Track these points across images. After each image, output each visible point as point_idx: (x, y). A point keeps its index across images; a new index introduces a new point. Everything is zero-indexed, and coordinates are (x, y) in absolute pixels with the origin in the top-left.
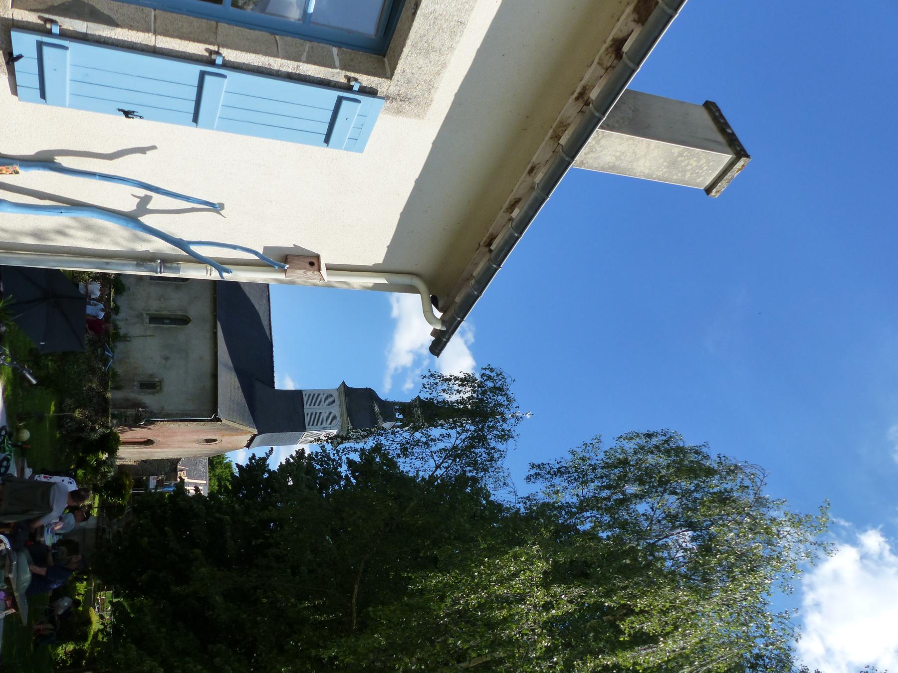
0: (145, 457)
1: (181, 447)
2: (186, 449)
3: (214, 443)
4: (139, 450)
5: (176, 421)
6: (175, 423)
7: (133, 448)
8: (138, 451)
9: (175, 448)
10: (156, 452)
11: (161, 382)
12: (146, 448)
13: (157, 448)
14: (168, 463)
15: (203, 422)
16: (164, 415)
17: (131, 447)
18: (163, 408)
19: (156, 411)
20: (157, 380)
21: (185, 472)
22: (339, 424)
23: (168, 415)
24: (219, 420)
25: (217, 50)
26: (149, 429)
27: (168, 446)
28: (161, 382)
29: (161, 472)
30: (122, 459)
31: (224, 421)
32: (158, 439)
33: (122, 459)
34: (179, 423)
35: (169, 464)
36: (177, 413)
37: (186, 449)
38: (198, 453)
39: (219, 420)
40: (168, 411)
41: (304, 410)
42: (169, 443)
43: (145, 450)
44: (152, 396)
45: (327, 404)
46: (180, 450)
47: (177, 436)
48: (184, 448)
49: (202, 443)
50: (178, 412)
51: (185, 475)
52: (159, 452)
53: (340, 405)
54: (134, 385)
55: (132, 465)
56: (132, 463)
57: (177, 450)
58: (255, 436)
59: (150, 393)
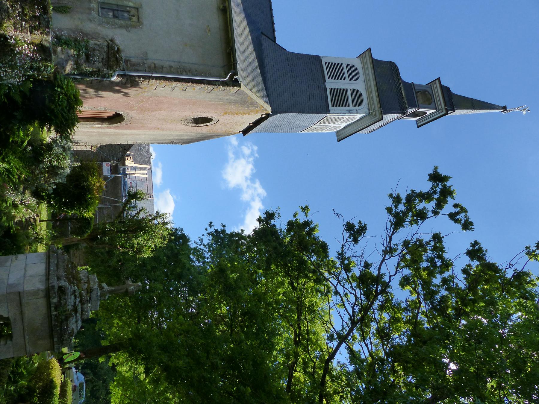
0: (106, 141)
1: (158, 129)
2: (165, 132)
3: (205, 124)
4: (100, 130)
5: (170, 79)
6: (168, 83)
7: (91, 128)
8: (98, 132)
9: (151, 129)
10: (123, 135)
11: (137, 9)
12: (110, 128)
13: (125, 129)
14: (119, 149)
15: (213, 85)
16: (150, 67)
17: (88, 126)
18: (146, 54)
19: (133, 60)
20: (131, 4)
21: (132, 157)
22: (367, 106)
23: (155, 68)
24: (235, 83)
25: (45, 223)
26: (126, 94)
27: (143, 127)
28: (137, 9)
29: (113, 157)
30: (77, 143)
31: (243, 88)
32: (133, 113)
33: (77, 143)
34: (175, 84)
35: (121, 150)
36: (171, 67)
37: (165, 132)
38: (176, 138)
39: (235, 83)
40: (156, 62)
41: (326, 84)
42: (145, 121)
43: (108, 130)
44: (124, 31)
45: (352, 78)
46: (157, 132)
47: (160, 110)
48: (163, 130)
49: (189, 124)
50: (173, 64)
51: (132, 160)
52: (126, 134)
53: (366, 82)
54: (90, 9)
55: (89, 151)
56: (88, 148)
57: (151, 132)
58: (268, 116)
59: (121, 27)
